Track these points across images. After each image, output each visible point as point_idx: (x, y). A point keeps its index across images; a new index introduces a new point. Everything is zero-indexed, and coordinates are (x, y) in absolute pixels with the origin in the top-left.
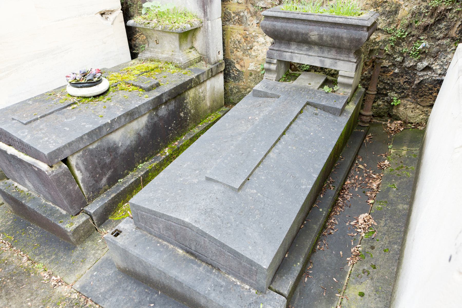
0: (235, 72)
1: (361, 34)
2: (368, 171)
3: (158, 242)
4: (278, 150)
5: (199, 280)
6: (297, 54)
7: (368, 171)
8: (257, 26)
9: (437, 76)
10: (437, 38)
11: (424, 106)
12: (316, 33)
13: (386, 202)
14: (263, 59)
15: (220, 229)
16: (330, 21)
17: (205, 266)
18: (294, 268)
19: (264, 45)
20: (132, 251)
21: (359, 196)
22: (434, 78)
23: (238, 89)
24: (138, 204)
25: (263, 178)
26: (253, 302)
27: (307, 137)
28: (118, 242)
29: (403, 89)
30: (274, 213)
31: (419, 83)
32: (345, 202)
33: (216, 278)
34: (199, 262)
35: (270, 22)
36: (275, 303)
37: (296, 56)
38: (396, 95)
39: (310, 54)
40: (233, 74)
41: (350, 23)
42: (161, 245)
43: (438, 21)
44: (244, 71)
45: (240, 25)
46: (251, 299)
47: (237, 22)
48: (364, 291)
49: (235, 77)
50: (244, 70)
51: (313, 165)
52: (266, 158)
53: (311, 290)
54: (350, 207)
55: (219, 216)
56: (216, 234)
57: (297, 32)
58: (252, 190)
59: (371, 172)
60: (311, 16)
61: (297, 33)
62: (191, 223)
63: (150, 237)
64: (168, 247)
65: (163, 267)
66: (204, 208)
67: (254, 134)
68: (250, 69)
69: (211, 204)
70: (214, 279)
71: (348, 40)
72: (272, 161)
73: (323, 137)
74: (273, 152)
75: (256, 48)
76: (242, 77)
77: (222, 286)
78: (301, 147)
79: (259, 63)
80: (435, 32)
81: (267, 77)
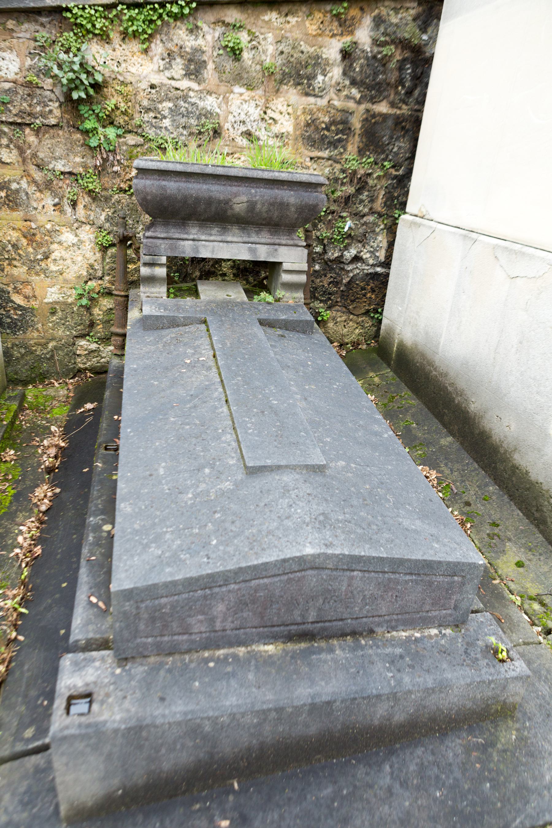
0: (12, 312)
1: (317, 197)
3: (207, 661)
5: (358, 672)
6: (204, 242)
8: (54, 210)
9: (369, 267)
10: (362, 213)
11: (358, 316)
12: (244, 198)
13: (421, 444)
14: (79, 277)
16: (266, 177)
17: (340, 645)
19: (76, 248)
20: (164, 716)
22: (365, 271)
23: (25, 348)
24: (150, 583)
26: (465, 646)
28: (105, 722)
29: (330, 294)
31: (349, 283)
33: (379, 651)
34: (323, 644)
35: (152, 182)
37: (204, 246)
38: (322, 305)
39: (229, 239)
40: (9, 317)
41: (299, 180)
42: (218, 660)
43: (359, 191)
44: (36, 307)
45: (12, 209)
46: (459, 645)
47: (5, 203)
48: (517, 559)
49: (15, 323)
50: (34, 304)
57: (210, 198)
60: (233, 169)
61: (209, 201)
62: (322, 551)
63: (173, 662)
64: (235, 657)
65: (270, 696)
68: (51, 300)
70: (377, 655)
71: (297, 209)
75: (59, 255)
76: (32, 321)
77: (402, 657)
79: (70, 286)
80: (358, 206)
81: (148, 294)
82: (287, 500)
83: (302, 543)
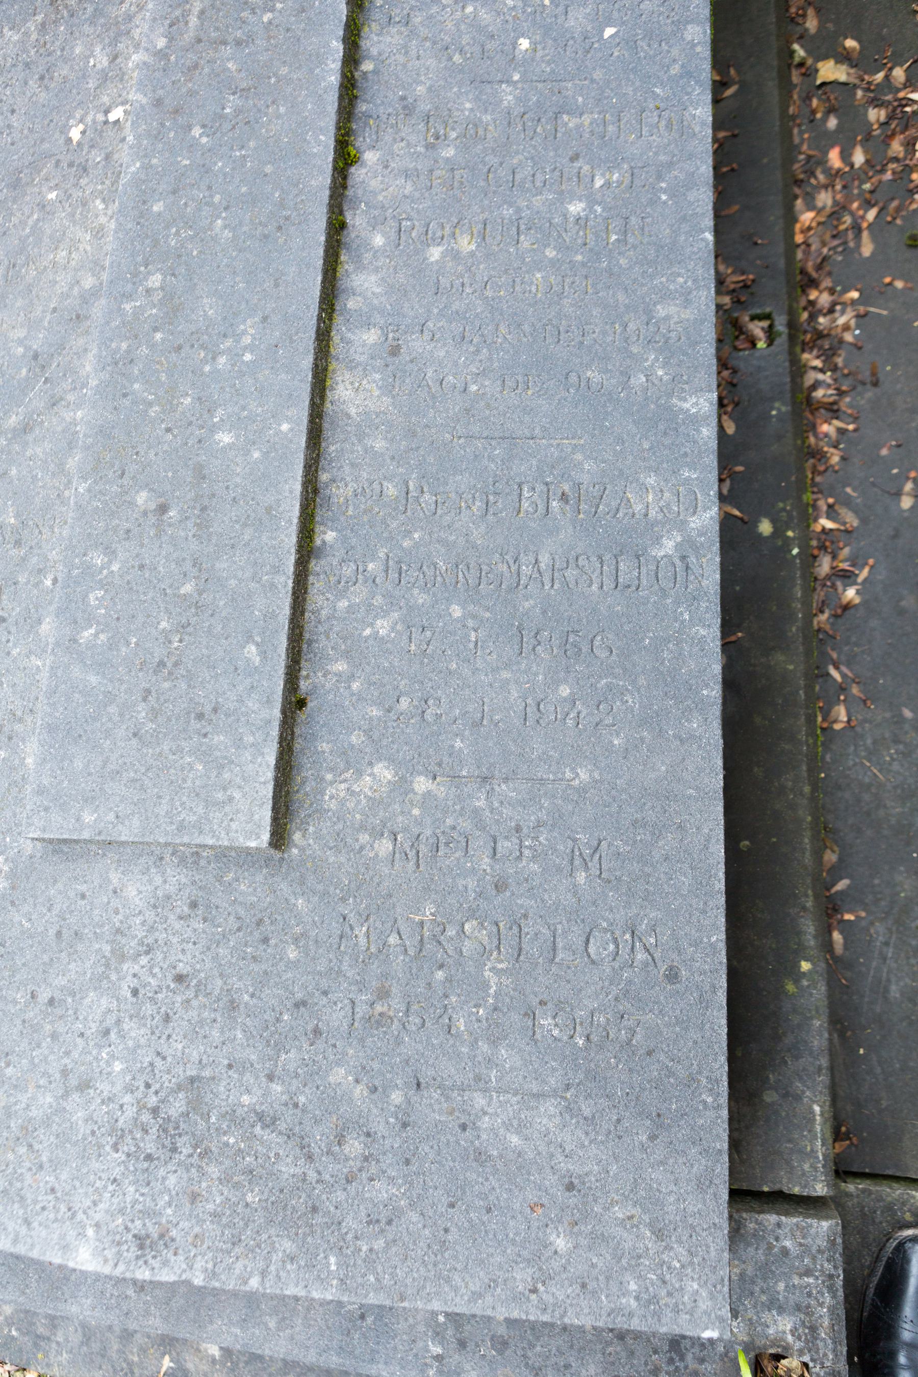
2: (880, 76)
4: (369, 325)
7: (880, 76)
15: (315, 1209)
18: (795, 1011)
21: (899, 284)
25: (383, 627)
27: (508, 96)
30: (581, 877)
32: (840, 361)
36: (796, 1281)
51: (649, 313)
52: (332, 447)
53: (886, 990)
54: (875, 384)
55: (260, 1117)
56: (310, 1266)
58: (359, 773)
59: (899, 74)
66: (141, 1106)
67: (155, 280)
69: (164, 1049)
72: (379, 445)
73: (609, 32)
74: (352, 366)
78: (508, 212)
82: (104, 1001)
83: (80, 1216)
